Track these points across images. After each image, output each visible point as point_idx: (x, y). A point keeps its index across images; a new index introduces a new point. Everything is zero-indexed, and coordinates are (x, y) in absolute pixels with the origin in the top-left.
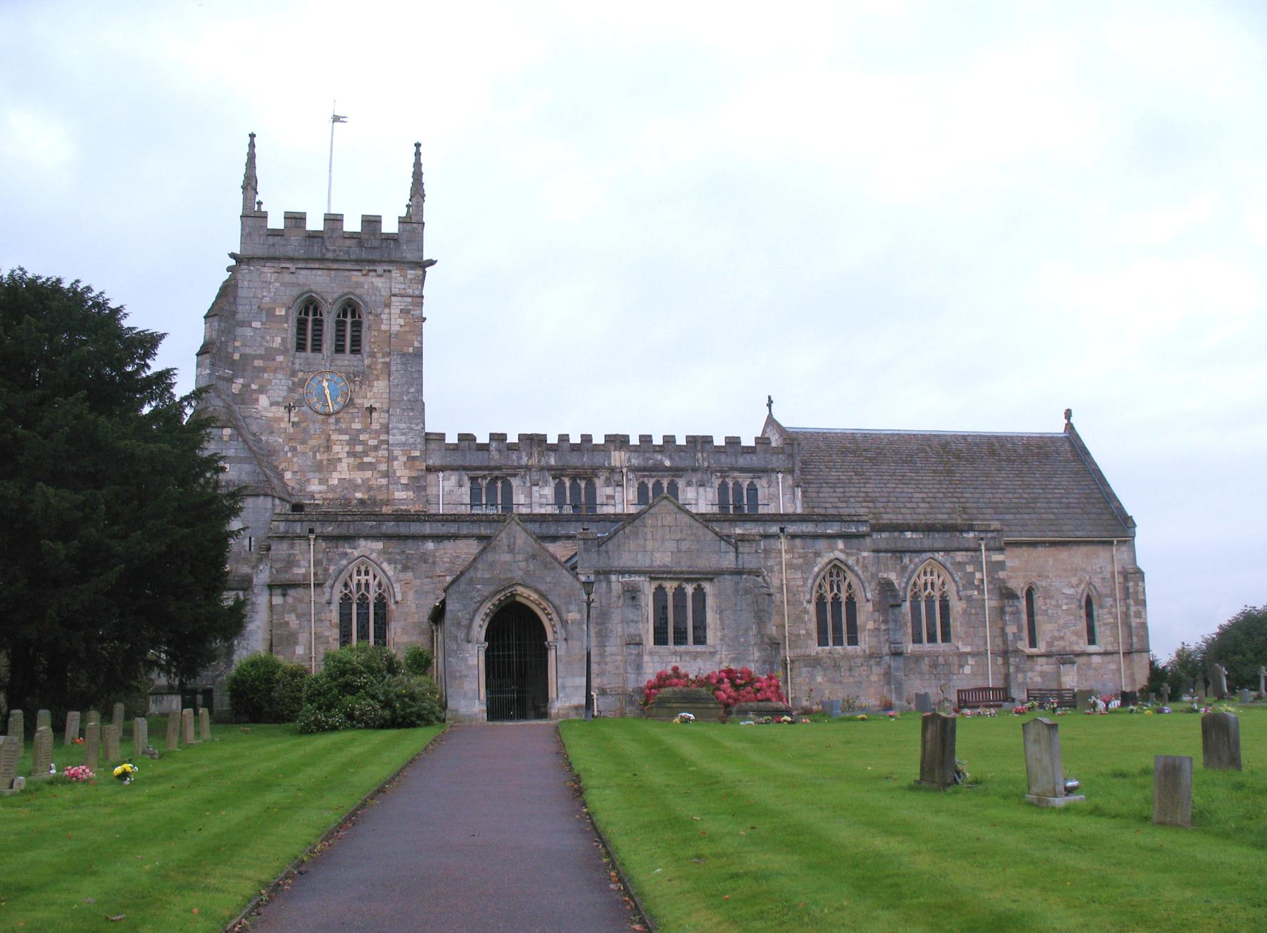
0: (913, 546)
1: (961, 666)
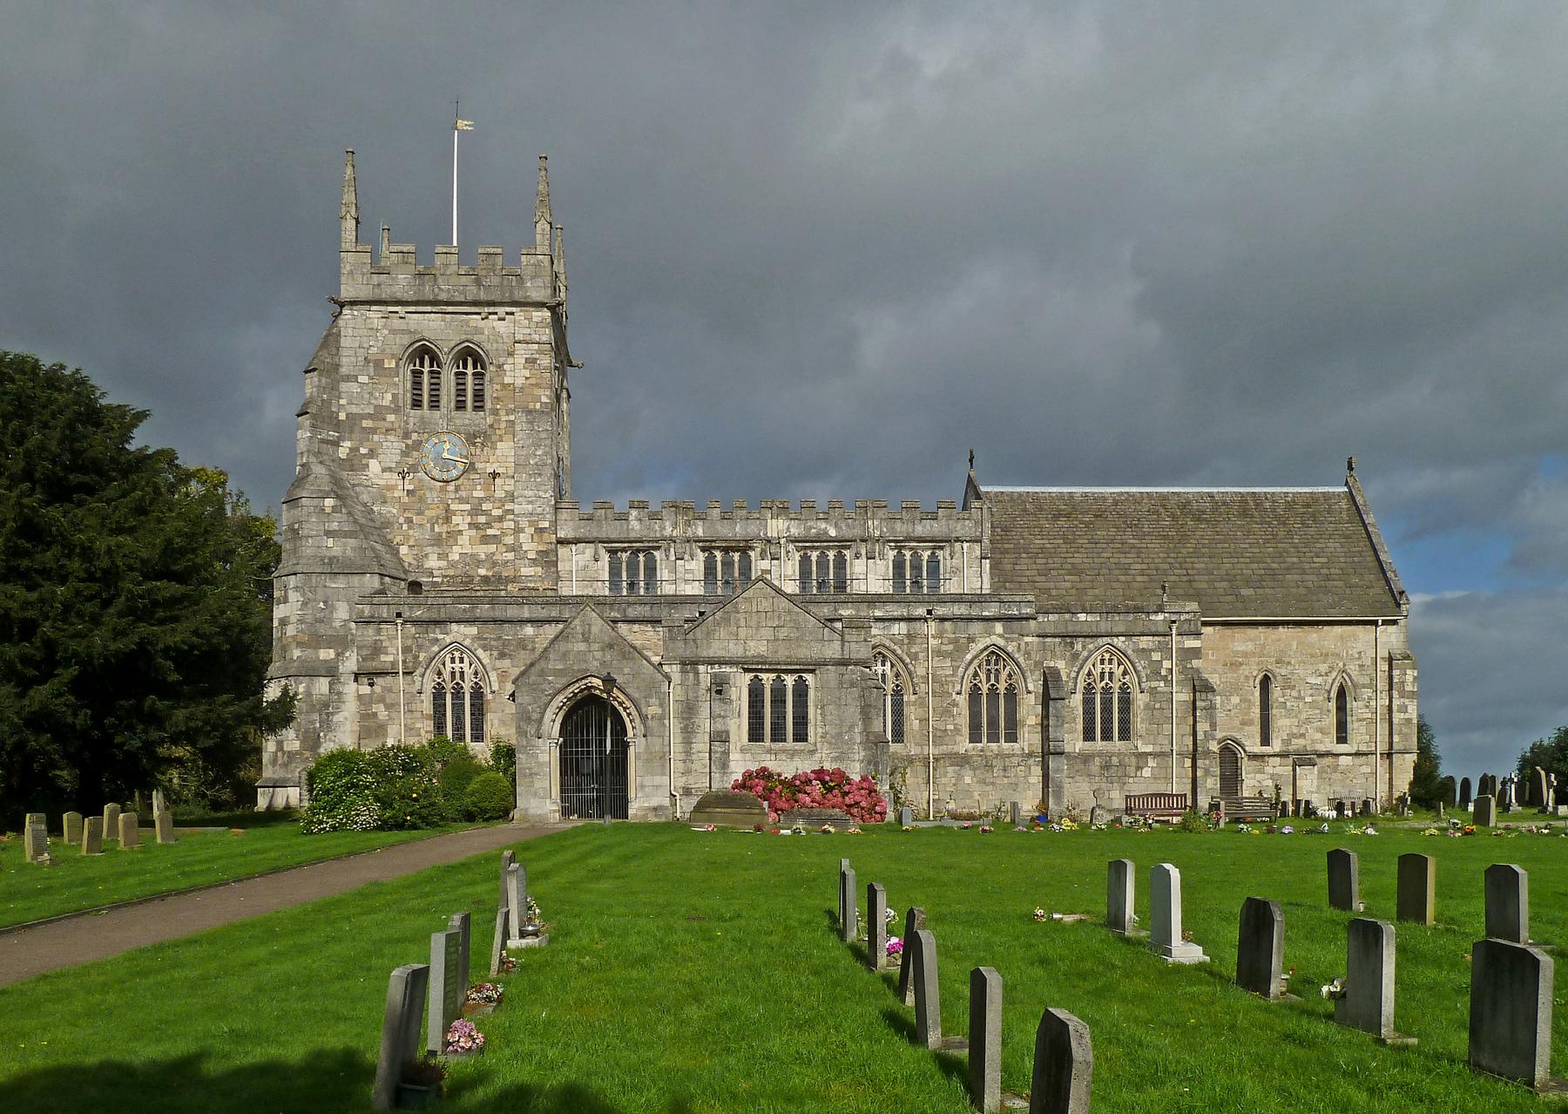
0: (1086, 630)
1: (1139, 768)
